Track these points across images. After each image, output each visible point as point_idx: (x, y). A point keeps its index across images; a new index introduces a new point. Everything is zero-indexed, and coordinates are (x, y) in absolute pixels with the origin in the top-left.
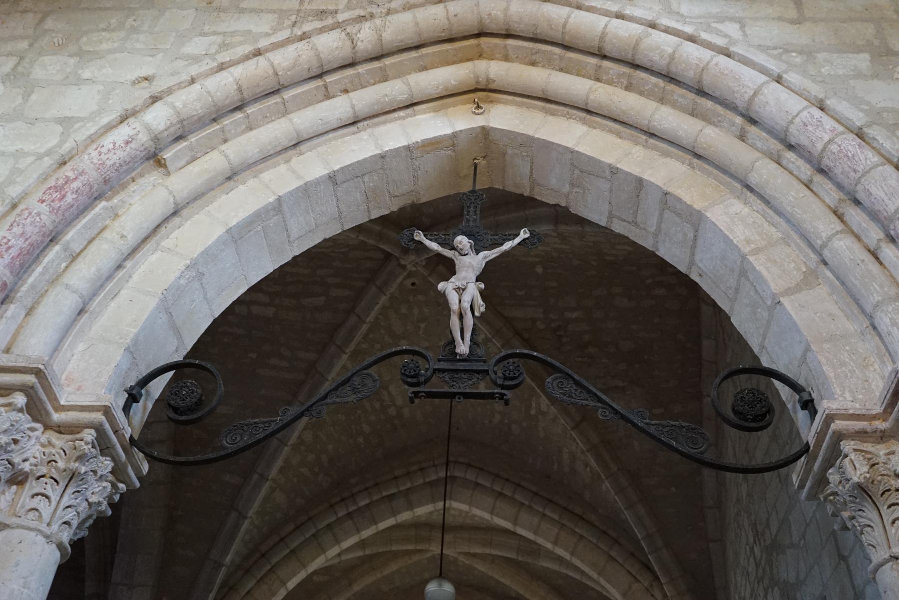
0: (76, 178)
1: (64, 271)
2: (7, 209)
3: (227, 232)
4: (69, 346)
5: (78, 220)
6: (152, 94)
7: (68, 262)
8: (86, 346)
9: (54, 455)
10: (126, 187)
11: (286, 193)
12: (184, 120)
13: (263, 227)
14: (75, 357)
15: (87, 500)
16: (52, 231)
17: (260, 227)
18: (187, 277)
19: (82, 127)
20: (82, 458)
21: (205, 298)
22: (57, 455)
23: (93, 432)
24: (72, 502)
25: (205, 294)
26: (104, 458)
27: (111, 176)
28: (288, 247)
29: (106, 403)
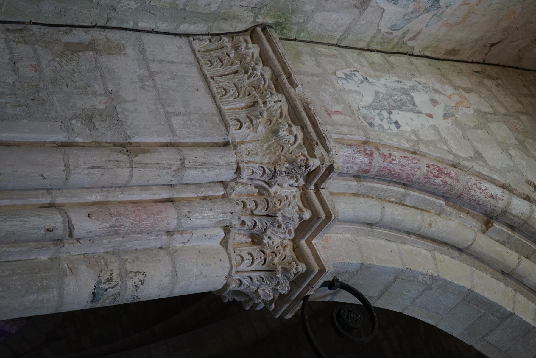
0: (452, 178)
1: (390, 201)
2: (411, 150)
3: (469, 290)
4: (347, 228)
5: (425, 193)
6: (530, 195)
7: (396, 201)
8: (350, 239)
9: (279, 253)
10: (461, 211)
11: (519, 317)
12: (527, 224)
13: (484, 313)
14: (341, 236)
15: (258, 288)
16: (413, 181)
17: (484, 311)
18: (425, 279)
19: (483, 166)
20: (285, 271)
21: (415, 299)
22: (280, 254)
23: (305, 269)
24: (255, 280)
25: (417, 298)
26: (289, 286)
27: (465, 198)
28: (478, 338)
29: (327, 268)
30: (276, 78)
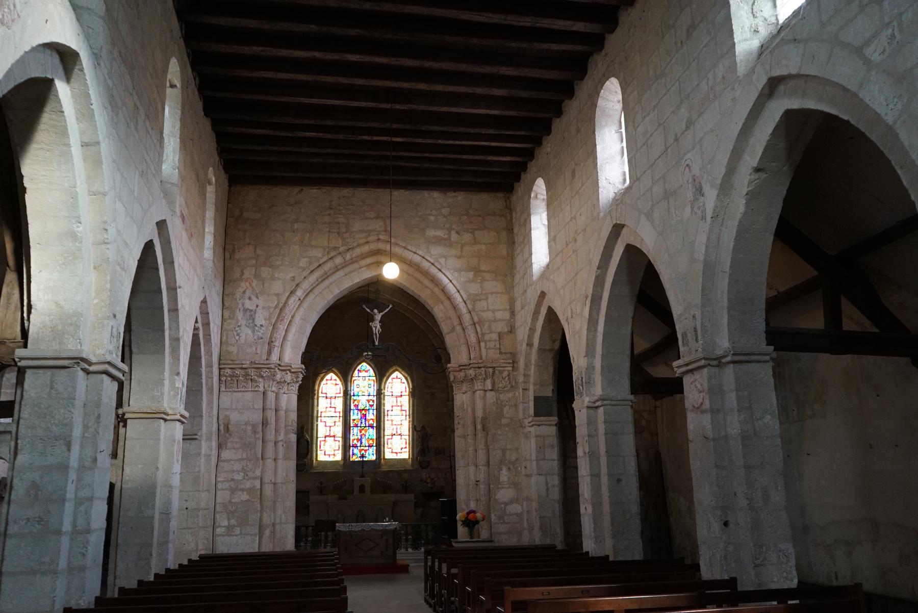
30: (242, 368)
